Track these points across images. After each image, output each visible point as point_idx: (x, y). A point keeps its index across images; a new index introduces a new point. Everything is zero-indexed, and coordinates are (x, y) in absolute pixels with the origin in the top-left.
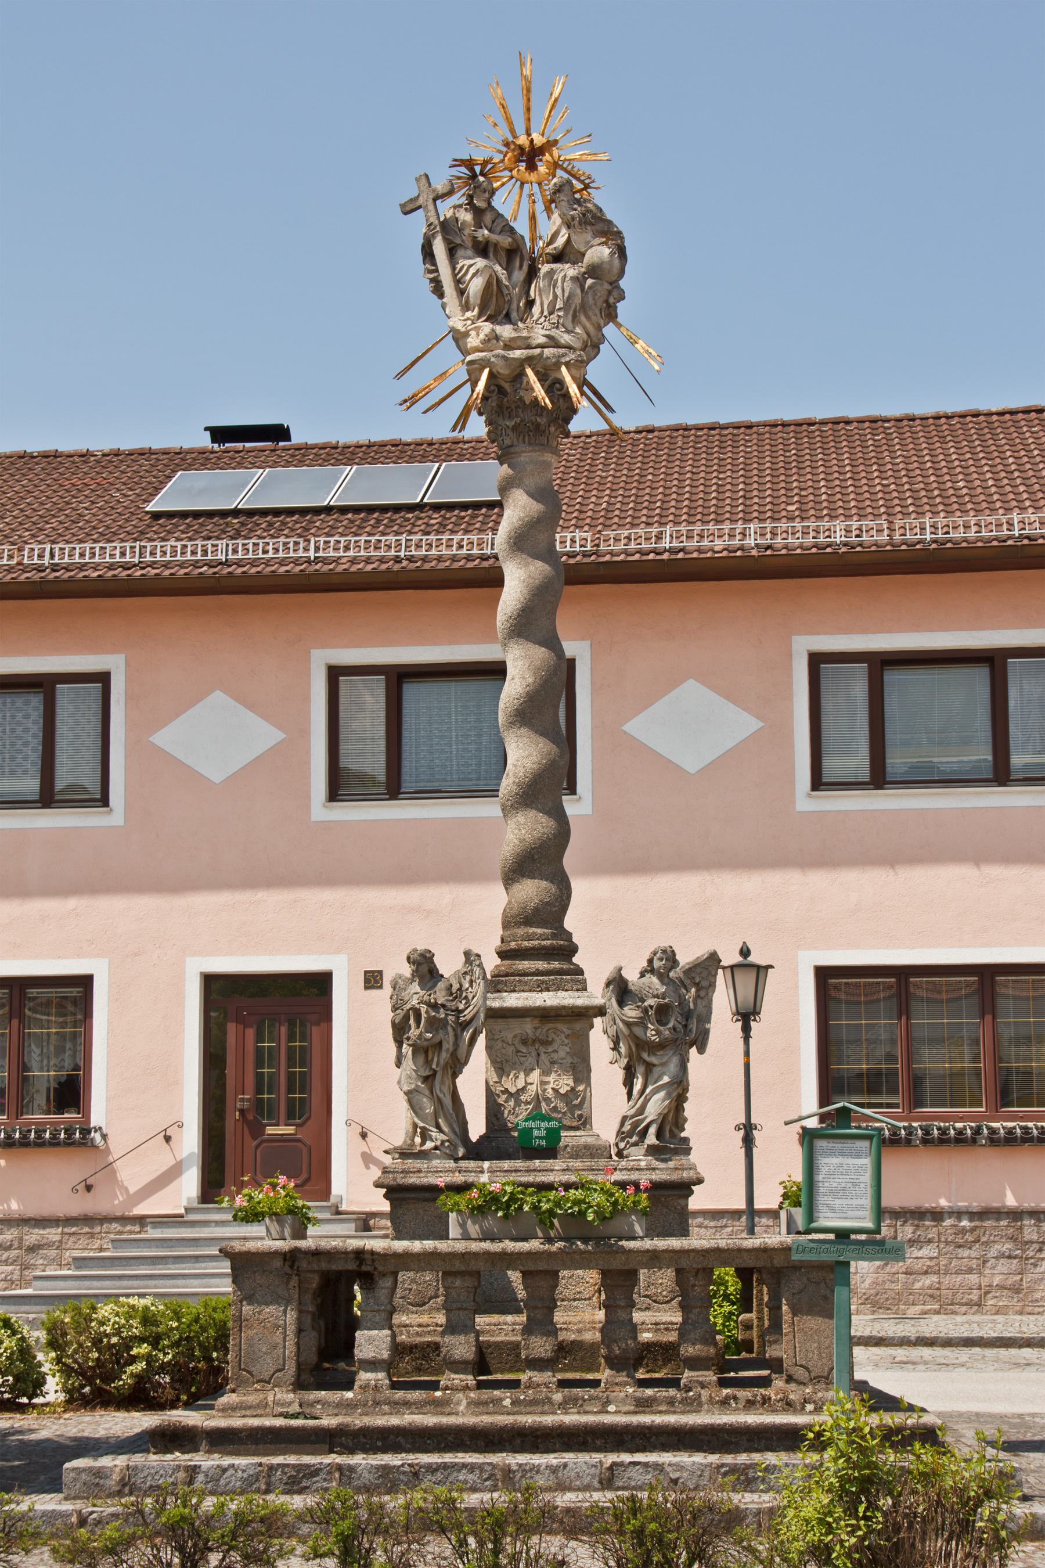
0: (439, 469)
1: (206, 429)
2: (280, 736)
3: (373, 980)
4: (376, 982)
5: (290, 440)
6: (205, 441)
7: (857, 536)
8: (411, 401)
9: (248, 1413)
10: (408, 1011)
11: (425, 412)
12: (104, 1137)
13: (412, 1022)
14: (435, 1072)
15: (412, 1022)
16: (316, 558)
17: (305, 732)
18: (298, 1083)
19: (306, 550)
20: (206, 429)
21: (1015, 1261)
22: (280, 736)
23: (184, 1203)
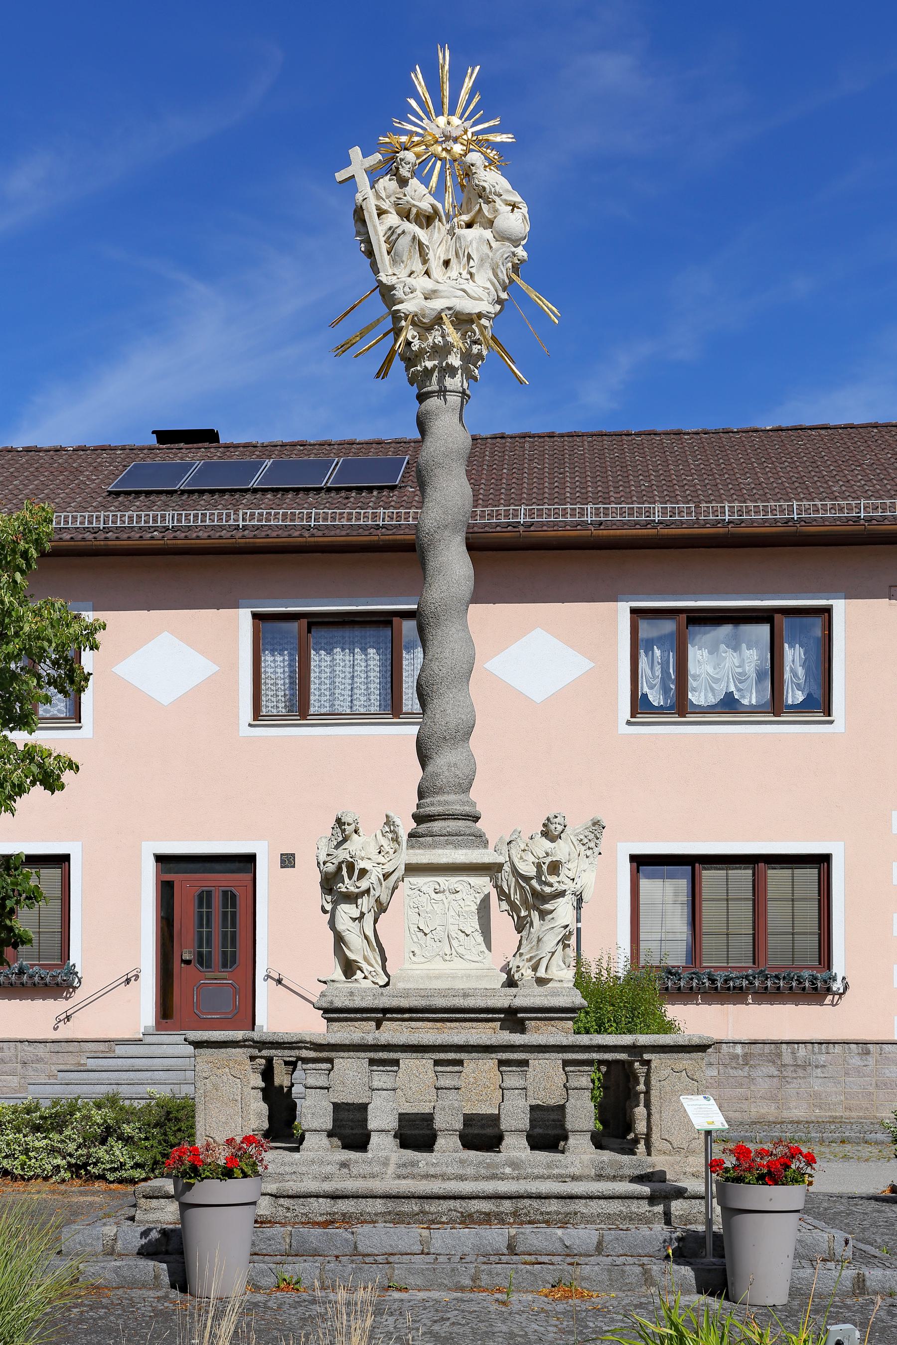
0: (338, 463)
1: (153, 432)
2: (215, 668)
3: (288, 861)
4: (290, 862)
5: (218, 442)
6: (153, 440)
7: (671, 516)
8: (344, 347)
9: (324, 1205)
10: (341, 863)
11: (356, 357)
12: (80, 981)
13: (344, 872)
14: (363, 914)
15: (344, 872)
16: (243, 526)
17: (235, 666)
18: (230, 939)
19: (236, 520)
20: (153, 432)
21: (775, 1080)
22: (215, 668)
23: (142, 1030)
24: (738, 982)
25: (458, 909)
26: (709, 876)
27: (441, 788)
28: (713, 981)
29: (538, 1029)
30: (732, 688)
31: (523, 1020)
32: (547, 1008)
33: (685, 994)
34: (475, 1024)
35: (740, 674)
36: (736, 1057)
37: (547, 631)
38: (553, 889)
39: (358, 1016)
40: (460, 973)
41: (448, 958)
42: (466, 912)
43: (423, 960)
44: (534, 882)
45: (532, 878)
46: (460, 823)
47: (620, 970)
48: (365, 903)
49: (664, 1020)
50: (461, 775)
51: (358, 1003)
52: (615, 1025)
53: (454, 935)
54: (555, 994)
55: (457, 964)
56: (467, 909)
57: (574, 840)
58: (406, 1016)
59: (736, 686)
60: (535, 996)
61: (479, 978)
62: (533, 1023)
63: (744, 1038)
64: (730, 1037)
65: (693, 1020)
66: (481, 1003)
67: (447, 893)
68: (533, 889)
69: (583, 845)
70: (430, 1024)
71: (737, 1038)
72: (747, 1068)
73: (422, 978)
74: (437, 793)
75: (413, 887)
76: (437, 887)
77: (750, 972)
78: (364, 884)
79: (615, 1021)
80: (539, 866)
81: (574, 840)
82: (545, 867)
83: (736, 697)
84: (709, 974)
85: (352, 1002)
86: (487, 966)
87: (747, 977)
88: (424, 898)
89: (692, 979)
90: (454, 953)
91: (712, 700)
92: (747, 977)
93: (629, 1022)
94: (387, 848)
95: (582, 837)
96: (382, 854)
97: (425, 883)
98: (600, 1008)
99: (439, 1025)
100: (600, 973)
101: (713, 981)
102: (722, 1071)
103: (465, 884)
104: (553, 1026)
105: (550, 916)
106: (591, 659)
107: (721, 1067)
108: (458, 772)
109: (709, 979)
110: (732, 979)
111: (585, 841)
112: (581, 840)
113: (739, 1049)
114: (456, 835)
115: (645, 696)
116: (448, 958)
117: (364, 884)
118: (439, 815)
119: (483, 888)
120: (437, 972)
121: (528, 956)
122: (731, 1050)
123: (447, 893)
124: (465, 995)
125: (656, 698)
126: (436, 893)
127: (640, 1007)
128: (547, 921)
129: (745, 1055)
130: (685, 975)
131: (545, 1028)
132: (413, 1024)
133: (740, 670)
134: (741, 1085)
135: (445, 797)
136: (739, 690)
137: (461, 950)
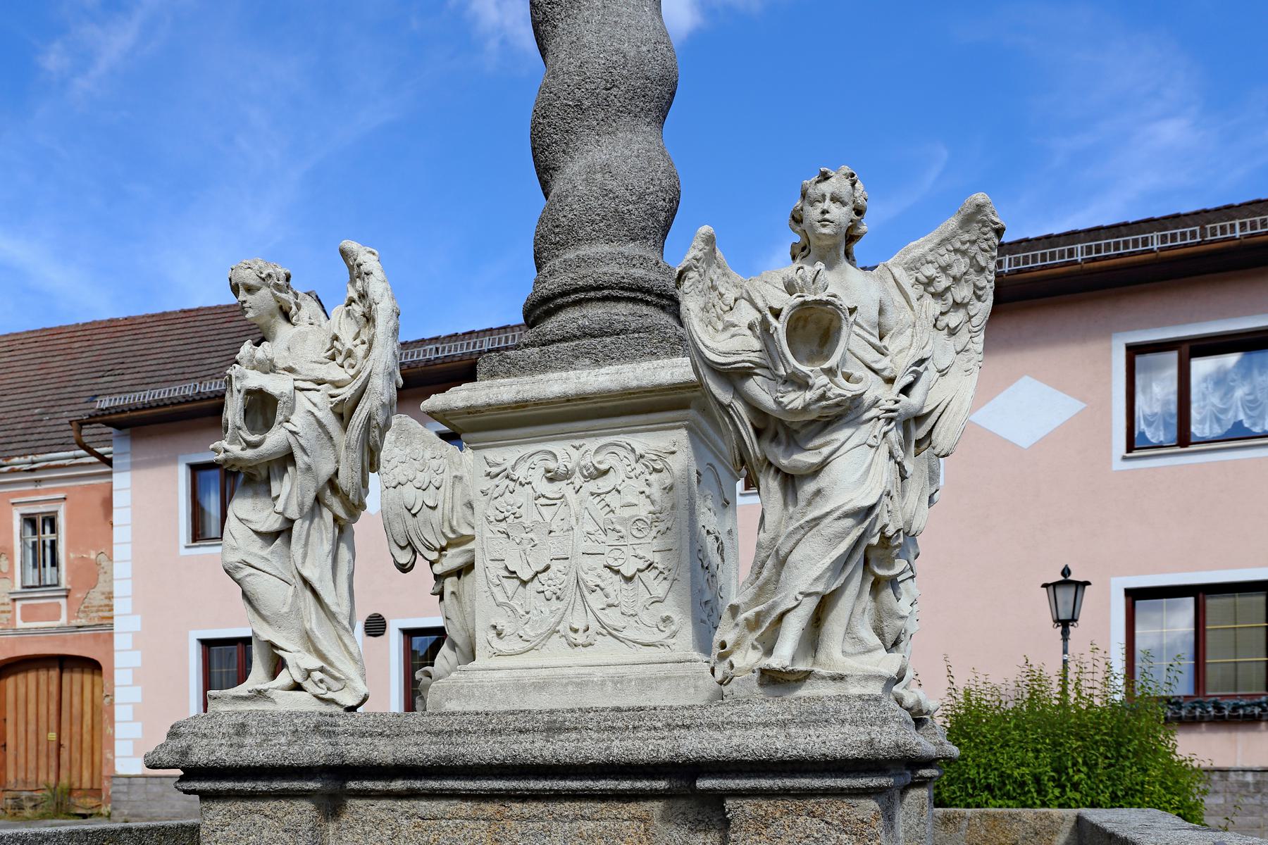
24: (1249, 710)
25: (601, 515)
26: (1212, 603)
27: (570, 230)
28: (1218, 707)
29: (764, 822)
30: (1241, 416)
31: (718, 798)
32: (782, 762)
33: (1191, 722)
34: (588, 808)
35: (1250, 401)
36: (1246, 785)
37: (1036, 378)
38: (809, 395)
39: (261, 786)
40: (598, 674)
41: (580, 638)
42: (623, 521)
43: (519, 645)
44: (756, 387)
45: (747, 373)
46: (622, 309)
47: (1096, 685)
48: (290, 491)
49: (1172, 761)
50: (621, 191)
51: (254, 753)
52: (1084, 769)
53: (591, 580)
54: (815, 717)
55: (606, 652)
56: (628, 512)
57: (907, 282)
58: (398, 785)
59: (1246, 414)
60: (746, 726)
61: (646, 683)
62: (749, 806)
63: (1256, 765)
64: (1239, 765)
65: (1197, 748)
66: (591, 748)
67: (578, 480)
68: (756, 410)
69: (938, 296)
70: (466, 807)
71: (1247, 765)
72: (1259, 796)
73: (502, 688)
74: (564, 245)
75: (495, 470)
76: (552, 465)
77: (1263, 699)
78: (274, 439)
79: (1085, 763)
80: (764, 331)
81: (907, 282)
82: (779, 327)
83: (1246, 425)
84: (1215, 702)
85: (233, 751)
86: (676, 656)
87: (1259, 705)
88: (523, 496)
89: (1194, 708)
90: (594, 626)
91: (1218, 431)
92: (1259, 705)
93: (1111, 765)
94: (347, 341)
95: (930, 271)
96: (339, 360)
97: (521, 459)
98: (1061, 744)
99: (490, 808)
100: (1064, 691)
101: (1218, 707)
102: (1229, 799)
103: (622, 453)
104: (811, 814)
105: (809, 488)
106: (1083, 400)
107: (1228, 795)
108: (612, 184)
109: (1214, 707)
110: (1242, 707)
111: (943, 282)
112: (930, 281)
113: (1249, 778)
114: (603, 334)
115: (1142, 434)
116: (580, 638)
117: (274, 439)
118: (564, 294)
119: (670, 460)
120: (544, 673)
121: (750, 613)
122: (1240, 778)
123: (578, 480)
124: (554, 729)
125: (1155, 435)
126: (551, 480)
127: (1130, 741)
128: (802, 503)
129: (1257, 784)
130: (1187, 704)
131: (786, 820)
132: (424, 806)
133: (1251, 398)
134: (1252, 813)
135: (585, 250)
136: (1250, 417)
137: (612, 618)
